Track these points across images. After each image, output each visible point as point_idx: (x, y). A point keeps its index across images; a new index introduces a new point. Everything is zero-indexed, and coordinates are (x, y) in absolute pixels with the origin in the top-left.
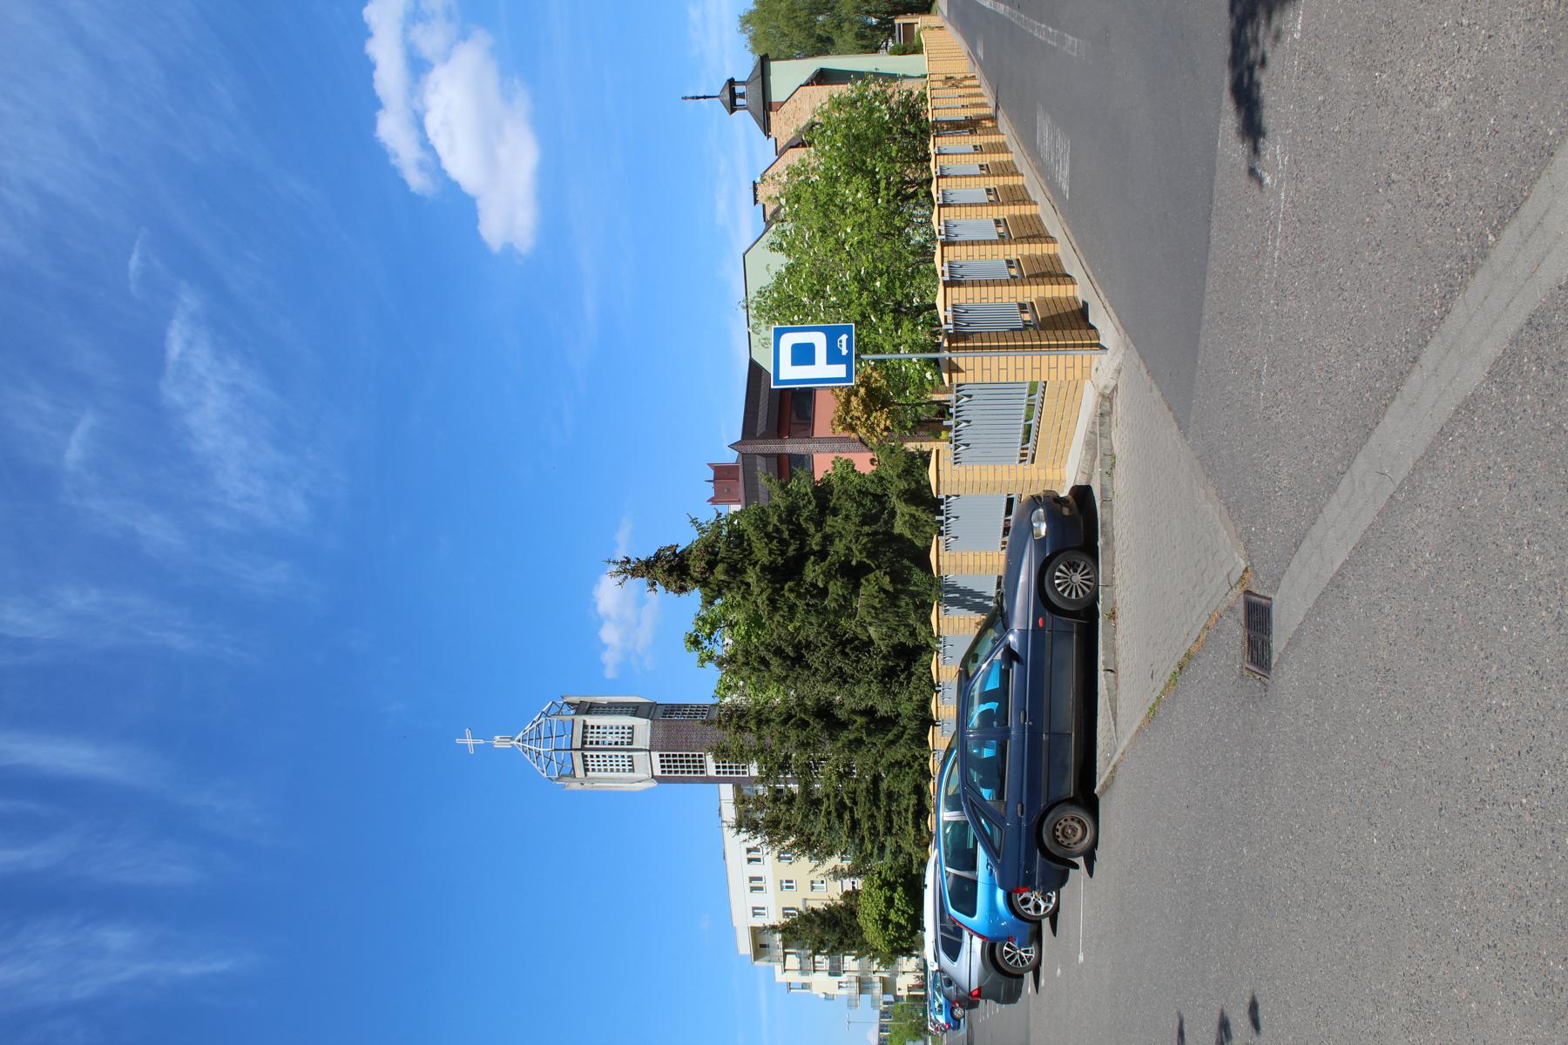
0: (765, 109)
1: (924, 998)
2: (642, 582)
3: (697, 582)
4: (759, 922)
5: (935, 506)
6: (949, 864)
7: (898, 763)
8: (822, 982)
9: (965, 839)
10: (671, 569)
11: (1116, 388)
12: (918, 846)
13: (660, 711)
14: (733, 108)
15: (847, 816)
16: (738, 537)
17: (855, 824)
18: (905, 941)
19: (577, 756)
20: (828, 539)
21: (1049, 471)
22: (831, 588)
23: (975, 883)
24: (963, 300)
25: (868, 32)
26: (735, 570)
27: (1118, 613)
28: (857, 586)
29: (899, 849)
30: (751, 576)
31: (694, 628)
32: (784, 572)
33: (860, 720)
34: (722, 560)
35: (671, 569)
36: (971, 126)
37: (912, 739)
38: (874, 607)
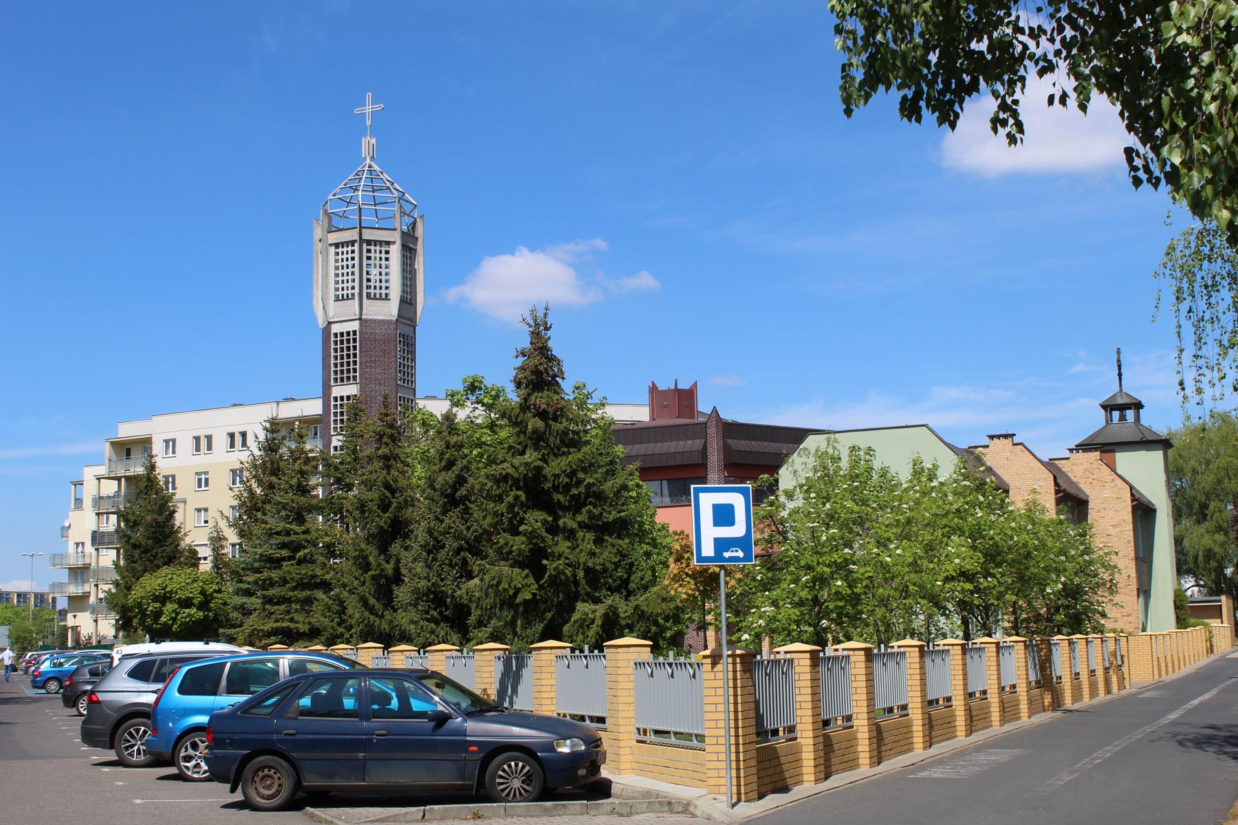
0: (1103, 447)
1: (63, 646)
2: (525, 343)
3: (526, 400)
4: (158, 448)
5: (598, 646)
6: (233, 664)
7: (343, 610)
8: (84, 523)
9: (259, 682)
10: (540, 373)
11: (694, 816)
12: (250, 635)
13: (407, 330)
14: (1108, 407)
15: (285, 553)
16: (574, 442)
17: (275, 563)
18: (133, 621)
19: (352, 235)
20: (570, 535)
21: (629, 758)
22: (519, 539)
23: (215, 693)
24: (798, 670)
25: (1213, 564)
26: (538, 439)
27: (478, 822)
28: (522, 566)
29: (246, 612)
30: (531, 456)
31: (489, 385)
32: (535, 490)
33: (389, 568)
34: (548, 426)
35: (540, 373)
36: (1046, 681)
37: (370, 626)
38: (499, 583)
